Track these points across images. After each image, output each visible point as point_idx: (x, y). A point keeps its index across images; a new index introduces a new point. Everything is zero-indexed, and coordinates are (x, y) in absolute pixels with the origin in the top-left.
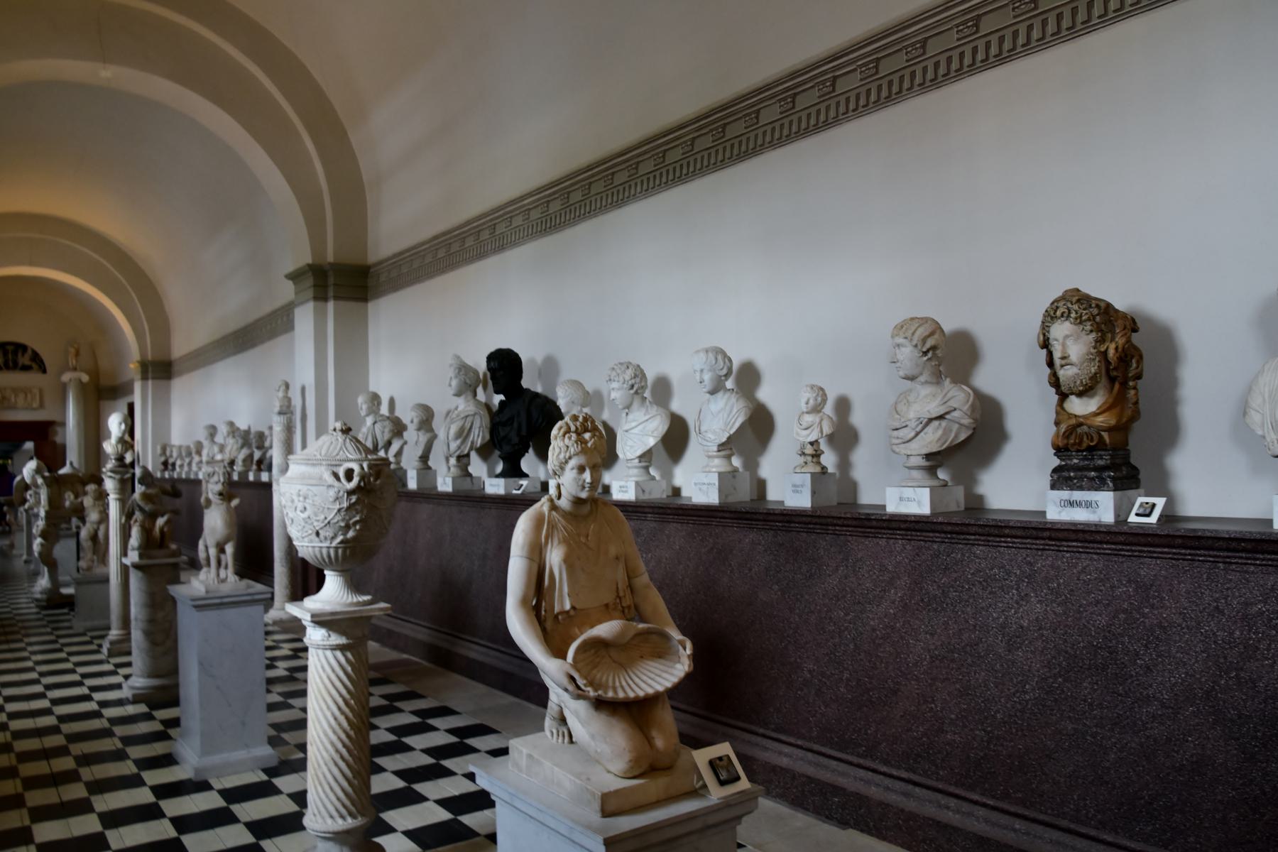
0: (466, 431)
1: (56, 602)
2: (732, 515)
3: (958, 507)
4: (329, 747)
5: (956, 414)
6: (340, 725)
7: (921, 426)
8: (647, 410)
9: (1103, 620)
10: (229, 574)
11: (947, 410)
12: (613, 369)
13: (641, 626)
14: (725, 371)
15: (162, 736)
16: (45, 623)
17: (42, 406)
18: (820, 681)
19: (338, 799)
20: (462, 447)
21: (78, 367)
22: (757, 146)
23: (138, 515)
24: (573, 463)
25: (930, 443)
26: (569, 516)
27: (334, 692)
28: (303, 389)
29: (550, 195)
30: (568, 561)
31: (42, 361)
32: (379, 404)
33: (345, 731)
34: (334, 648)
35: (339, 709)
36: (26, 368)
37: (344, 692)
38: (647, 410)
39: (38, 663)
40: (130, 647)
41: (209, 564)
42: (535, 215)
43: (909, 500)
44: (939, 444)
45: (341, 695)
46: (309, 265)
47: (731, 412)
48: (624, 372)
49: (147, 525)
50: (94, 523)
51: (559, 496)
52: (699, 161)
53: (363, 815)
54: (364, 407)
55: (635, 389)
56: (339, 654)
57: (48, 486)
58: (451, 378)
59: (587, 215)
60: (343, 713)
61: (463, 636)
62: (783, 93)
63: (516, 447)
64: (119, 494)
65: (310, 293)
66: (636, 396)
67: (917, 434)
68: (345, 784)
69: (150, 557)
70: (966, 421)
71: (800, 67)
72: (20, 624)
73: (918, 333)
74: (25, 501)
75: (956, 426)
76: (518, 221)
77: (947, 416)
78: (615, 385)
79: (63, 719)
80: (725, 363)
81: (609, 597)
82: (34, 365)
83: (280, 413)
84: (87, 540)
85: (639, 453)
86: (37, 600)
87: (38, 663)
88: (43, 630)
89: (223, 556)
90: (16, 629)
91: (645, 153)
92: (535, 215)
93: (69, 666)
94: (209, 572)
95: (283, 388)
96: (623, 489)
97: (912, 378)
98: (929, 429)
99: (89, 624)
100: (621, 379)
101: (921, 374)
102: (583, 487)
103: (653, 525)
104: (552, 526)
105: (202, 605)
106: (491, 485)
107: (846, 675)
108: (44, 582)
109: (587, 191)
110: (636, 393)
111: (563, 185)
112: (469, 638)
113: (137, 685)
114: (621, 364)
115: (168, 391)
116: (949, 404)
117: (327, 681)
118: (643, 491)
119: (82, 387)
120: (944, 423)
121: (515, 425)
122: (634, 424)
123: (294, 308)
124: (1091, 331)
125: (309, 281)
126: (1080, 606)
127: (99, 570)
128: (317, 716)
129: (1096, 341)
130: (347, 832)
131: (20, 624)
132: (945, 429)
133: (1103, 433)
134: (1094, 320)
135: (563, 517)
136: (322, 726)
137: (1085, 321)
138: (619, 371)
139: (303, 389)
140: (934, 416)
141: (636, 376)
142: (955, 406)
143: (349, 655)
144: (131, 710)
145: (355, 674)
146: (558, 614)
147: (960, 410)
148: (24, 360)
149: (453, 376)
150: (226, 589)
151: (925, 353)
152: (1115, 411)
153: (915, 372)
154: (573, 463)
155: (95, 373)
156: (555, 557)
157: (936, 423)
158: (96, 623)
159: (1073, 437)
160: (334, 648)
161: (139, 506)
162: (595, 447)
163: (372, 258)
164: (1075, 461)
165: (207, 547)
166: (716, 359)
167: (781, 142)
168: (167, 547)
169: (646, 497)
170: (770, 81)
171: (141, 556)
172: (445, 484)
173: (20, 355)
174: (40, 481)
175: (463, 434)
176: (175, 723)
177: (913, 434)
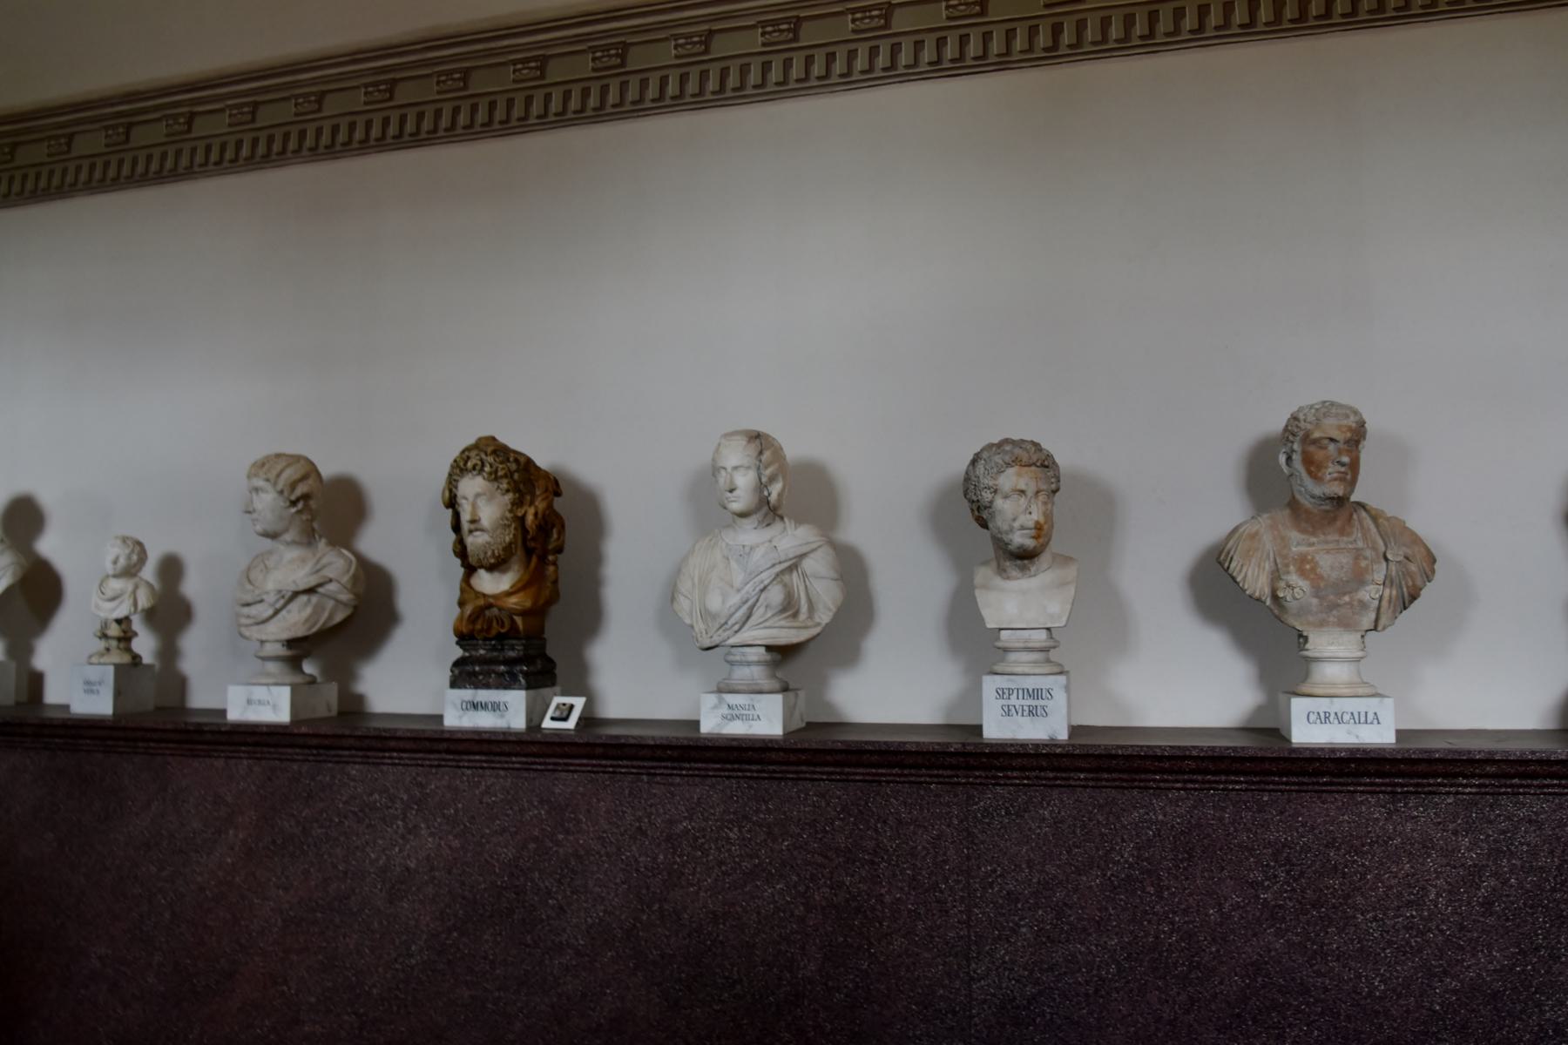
5: (332, 587)
44: (307, 625)
67: (277, 612)
75: (330, 604)
77: (321, 590)
98: (294, 606)
101: (286, 530)
120: (314, 599)
124: (508, 491)
134: (512, 477)
142: (331, 575)
147: (339, 582)
151: (294, 503)
157: (304, 598)
164: (482, 652)
177: (270, 612)
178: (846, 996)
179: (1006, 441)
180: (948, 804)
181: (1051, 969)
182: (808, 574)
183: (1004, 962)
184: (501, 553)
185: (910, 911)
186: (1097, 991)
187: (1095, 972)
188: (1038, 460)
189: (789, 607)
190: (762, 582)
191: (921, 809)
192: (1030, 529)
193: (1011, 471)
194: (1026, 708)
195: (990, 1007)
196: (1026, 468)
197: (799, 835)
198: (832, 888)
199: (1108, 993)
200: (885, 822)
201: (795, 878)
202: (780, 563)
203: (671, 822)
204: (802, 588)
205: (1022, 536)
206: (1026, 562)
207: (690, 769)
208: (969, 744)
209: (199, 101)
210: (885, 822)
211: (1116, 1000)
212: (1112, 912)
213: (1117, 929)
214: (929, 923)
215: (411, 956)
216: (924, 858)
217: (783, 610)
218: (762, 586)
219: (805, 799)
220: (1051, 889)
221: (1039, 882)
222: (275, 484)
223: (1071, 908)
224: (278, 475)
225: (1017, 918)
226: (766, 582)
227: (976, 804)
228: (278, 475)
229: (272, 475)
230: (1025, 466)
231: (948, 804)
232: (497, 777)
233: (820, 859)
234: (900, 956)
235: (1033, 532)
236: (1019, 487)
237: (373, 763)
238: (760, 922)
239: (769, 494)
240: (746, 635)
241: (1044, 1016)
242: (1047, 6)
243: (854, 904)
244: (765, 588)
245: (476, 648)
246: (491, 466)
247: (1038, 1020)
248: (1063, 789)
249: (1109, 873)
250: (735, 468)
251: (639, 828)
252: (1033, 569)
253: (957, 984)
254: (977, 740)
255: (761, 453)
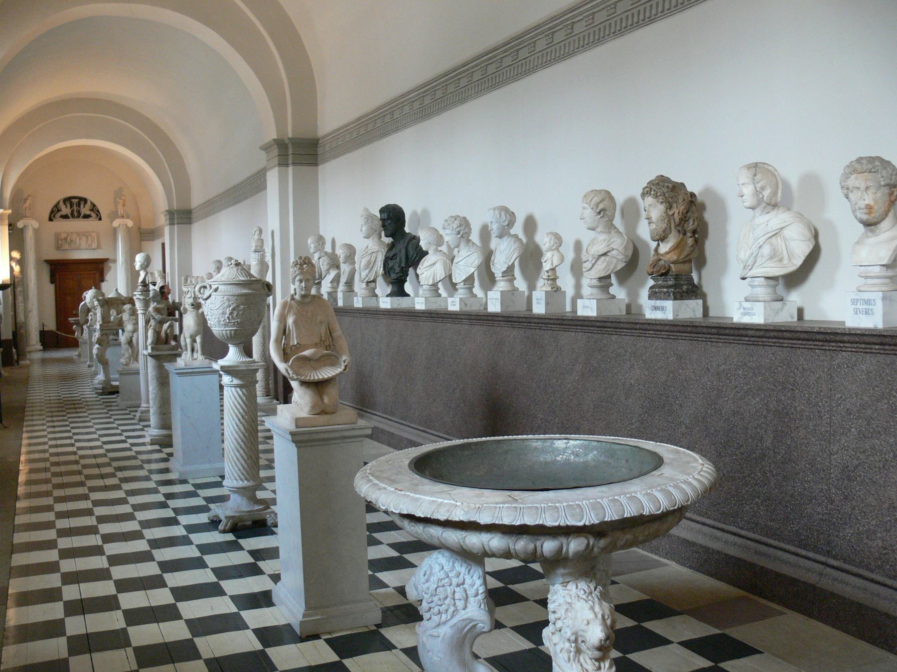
0: (372, 264)
1: (110, 391)
2: (503, 319)
3: (621, 312)
4: (234, 440)
5: (614, 252)
6: (239, 429)
7: (594, 260)
8: (469, 249)
9: (664, 378)
10: (199, 356)
11: (608, 250)
12: (446, 220)
13: (326, 352)
14: (506, 223)
15: (166, 460)
16: (101, 403)
17: (99, 247)
18: (545, 425)
19: (239, 470)
20: (369, 275)
21: (125, 216)
22: (646, 18)
23: (152, 322)
24: (297, 278)
25: (599, 271)
26: (300, 303)
27: (236, 411)
28: (273, 233)
29: (424, 92)
30: (295, 322)
31: (98, 211)
32: (324, 243)
33: (242, 433)
34: (236, 386)
35: (239, 420)
36: (87, 217)
37: (242, 411)
38: (469, 249)
39: (98, 429)
40: (149, 416)
41: (186, 349)
42: (416, 105)
43: (588, 307)
44: (604, 272)
45: (240, 413)
46: (274, 140)
47: (510, 250)
48: (453, 223)
49: (157, 329)
50: (129, 332)
51: (296, 294)
52: (642, 12)
53: (253, 481)
54: (312, 246)
55: (461, 234)
56: (238, 389)
57: (101, 307)
58: (362, 225)
59: (612, 35)
60: (241, 423)
61: (369, 410)
62: (547, 31)
63: (399, 275)
64: (588, 577)
65: (276, 161)
66: (462, 239)
67: (593, 265)
68: (243, 462)
69: (158, 350)
70: (620, 257)
71: (555, 14)
72: (85, 403)
73: (594, 200)
74: (87, 321)
75: (614, 261)
76: (407, 109)
77: (609, 254)
78: (448, 231)
79: (108, 451)
80: (506, 217)
81: (317, 340)
82: (93, 214)
83: (255, 251)
84: (125, 344)
85: (464, 278)
86: (96, 389)
87: (98, 429)
88: (100, 407)
89: (195, 344)
90: (81, 406)
91: (477, 65)
92: (416, 105)
93: (115, 425)
94: (186, 354)
95: (257, 232)
96: (453, 304)
97: (593, 229)
98: (599, 262)
99: (129, 403)
100: (451, 227)
101: (597, 227)
102: (302, 290)
103: (466, 327)
104: (291, 307)
105: (182, 374)
106: (383, 302)
107: (557, 420)
108: (101, 377)
109: (445, 91)
110: (462, 237)
111: (432, 85)
112: (371, 411)
113: (154, 433)
114: (452, 217)
115: (190, 232)
116: (611, 246)
117: (233, 405)
118: (466, 305)
119: (128, 230)
120: (607, 258)
121: (398, 259)
122: (461, 259)
123: (266, 172)
124: (662, 202)
125: (275, 152)
126: (655, 370)
127: (133, 366)
128: (228, 424)
129: (667, 209)
130: (244, 488)
131: (85, 403)
132: (608, 262)
133: (671, 265)
134: (664, 195)
135: (297, 303)
136: (230, 430)
137: (660, 196)
138: (449, 222)
139: (273, 233)
140: (600, 254)
141: (461, 225)
142: (614, 247)
143: (244, 390)
144: (149, 448)
145: (248, 402)
146: (292, 346)
147: (617, 250)
148: (85, 210)
149: (363, 223)
150: (196, 364)
151: (599, 213)
152: (677, 251)
153: (593, 225)
154: (297, 278)
155: (138, 220)
156: (290, 320)
157: (603, 258)
158: (133, 402)
159: (656, 267)
160: (236, 386)
161: (152, 316)
162: (307, 271)
163: (321, 133)
164: (660, 282)
165: (185, 338)
166: (500, 215)
167: (684, 7)
168: (170, 344)
169: (468, 309)
170: (541, 22)
171: (152, 349)
172: (358, 303)
173: (82, 206)
174: (96, 303)
175: (370, 265)
176: (171, 455)
177: (590, 266)
178: (782, 457)
179: (879, 159)
180: (823, 361)
181: (864, 452)
182: (787, 237)
183: (845, 446)
184: (662, 233)
185: (807, 416)
186: (884, 466)
187: (883, 456)
188: (867, 169)
189: (774, 256)
190: (759, 243)
191: (812, 363)
192: (863, 209)
193: (853, 177)
194: (864, 310)
195: (838, 470)
196: (861, 175)
197: (765, 374)
198: (777, 402)
199: (889, 468)
200: (798, 369)
201: (763, 396)
202: (768, 233)
203: (718, 365)
204: (783, 245)
205: (861, 213)
206: (873, 227)
207: (723, 339)
208: (822, 328)
209: (573, 17)
210: (798, 369)
211: (892, 472)
212: (892, 423)
213: (894, 434)
214: (814, 423)
215: (632, 424)
216: (813, 388)
217: (771, 258)
218: (759, 246)
219: (767, 356)
220: (865, 409)
221: (860, 405)
222: (590, 205)
223: (873, 420)
224: (591, 201)
225: (850, 424)
226: (761, 244)
227: (835, 361)
228: (591, 201)
229: (588, 202)
230: (860, 173)
231: (823, 361)
232: (659, 341)
233: (772, 387)
234: (803, 439)
235: (865, 211)
236: (855, 186)
237: (594, 327)
238: (750, 417)
239: (763, 197)
240: (754, 272)
241: (861, 477)
242: (632, 4)
243: (785, 411)
244: (760, 247)
245: (658, 281)
246: (654, 191)
247: (858, 478)
248: (872, 354)
249: (891, 402)
250: (743, 184)
251: (707, 368)
252: (878, 231)
253: (825, 456)
254: (843, 327)
255: (755, 175)
